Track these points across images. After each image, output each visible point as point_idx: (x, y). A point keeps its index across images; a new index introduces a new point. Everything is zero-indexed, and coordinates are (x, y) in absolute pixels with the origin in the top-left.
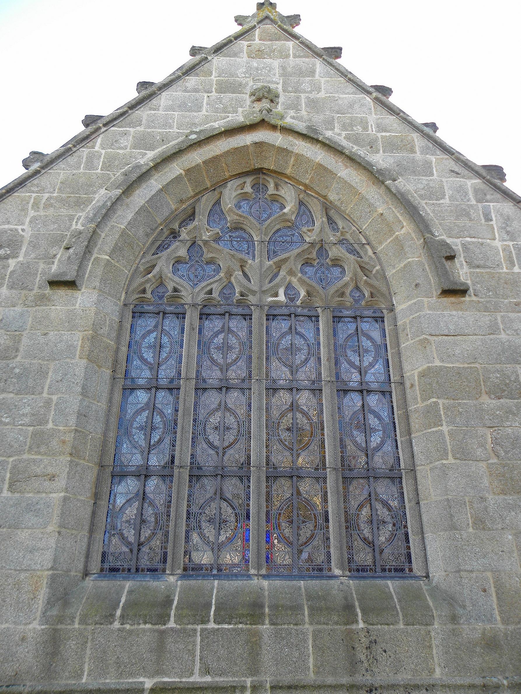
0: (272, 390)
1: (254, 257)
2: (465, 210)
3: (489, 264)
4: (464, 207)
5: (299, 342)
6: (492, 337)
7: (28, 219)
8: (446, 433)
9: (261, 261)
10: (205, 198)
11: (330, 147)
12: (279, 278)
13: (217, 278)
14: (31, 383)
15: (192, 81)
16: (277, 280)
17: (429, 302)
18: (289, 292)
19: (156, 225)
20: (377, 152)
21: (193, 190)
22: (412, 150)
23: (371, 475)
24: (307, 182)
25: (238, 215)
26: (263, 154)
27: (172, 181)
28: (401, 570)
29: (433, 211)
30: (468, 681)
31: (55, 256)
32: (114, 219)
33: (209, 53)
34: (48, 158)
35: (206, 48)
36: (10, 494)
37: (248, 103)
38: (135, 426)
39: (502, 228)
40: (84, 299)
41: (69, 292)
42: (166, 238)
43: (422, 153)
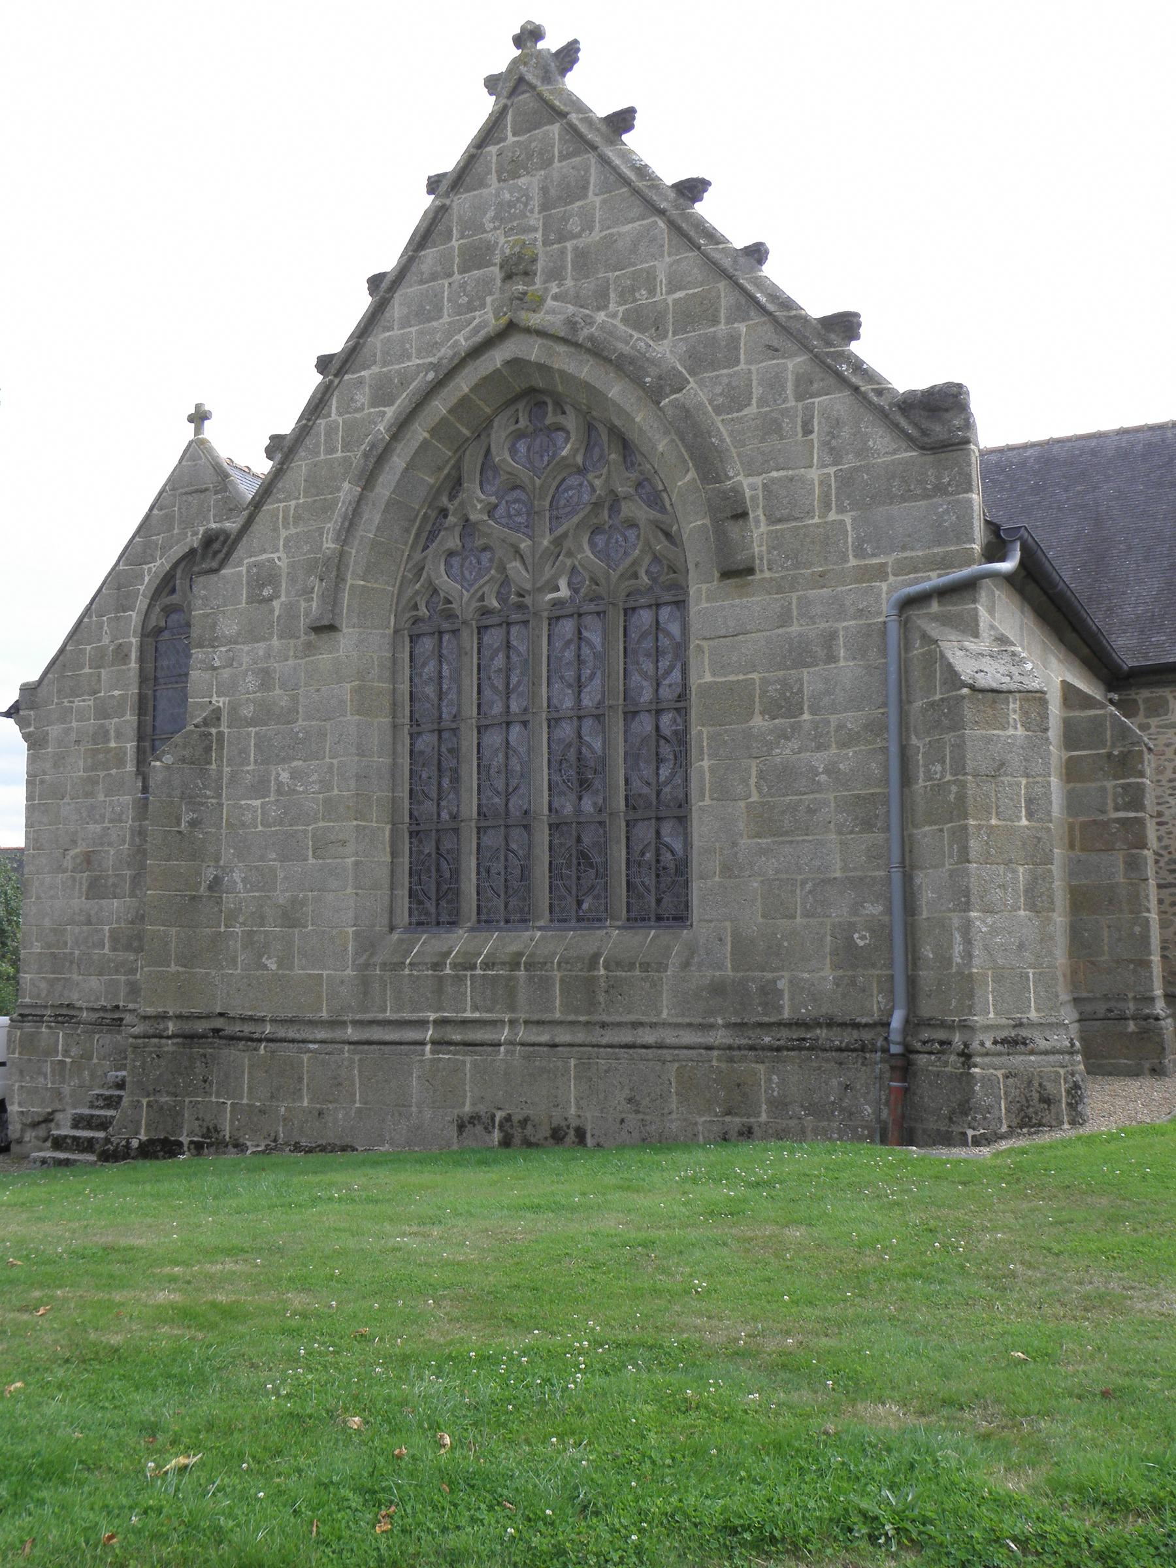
2: (775, 421)
4: (774, 415)
6: (780, 631)
8: (706, 769)
10: (468, 452)
11: (596, 351)
15: (430, 254)
17: (708, 589)
21: (449, 450)
27: (417, 453)
29: (731, 434)
30: (688, 1020)
32: (362, 527)
35: (445, 174)
36: (314, 861)
40: (347, 641)
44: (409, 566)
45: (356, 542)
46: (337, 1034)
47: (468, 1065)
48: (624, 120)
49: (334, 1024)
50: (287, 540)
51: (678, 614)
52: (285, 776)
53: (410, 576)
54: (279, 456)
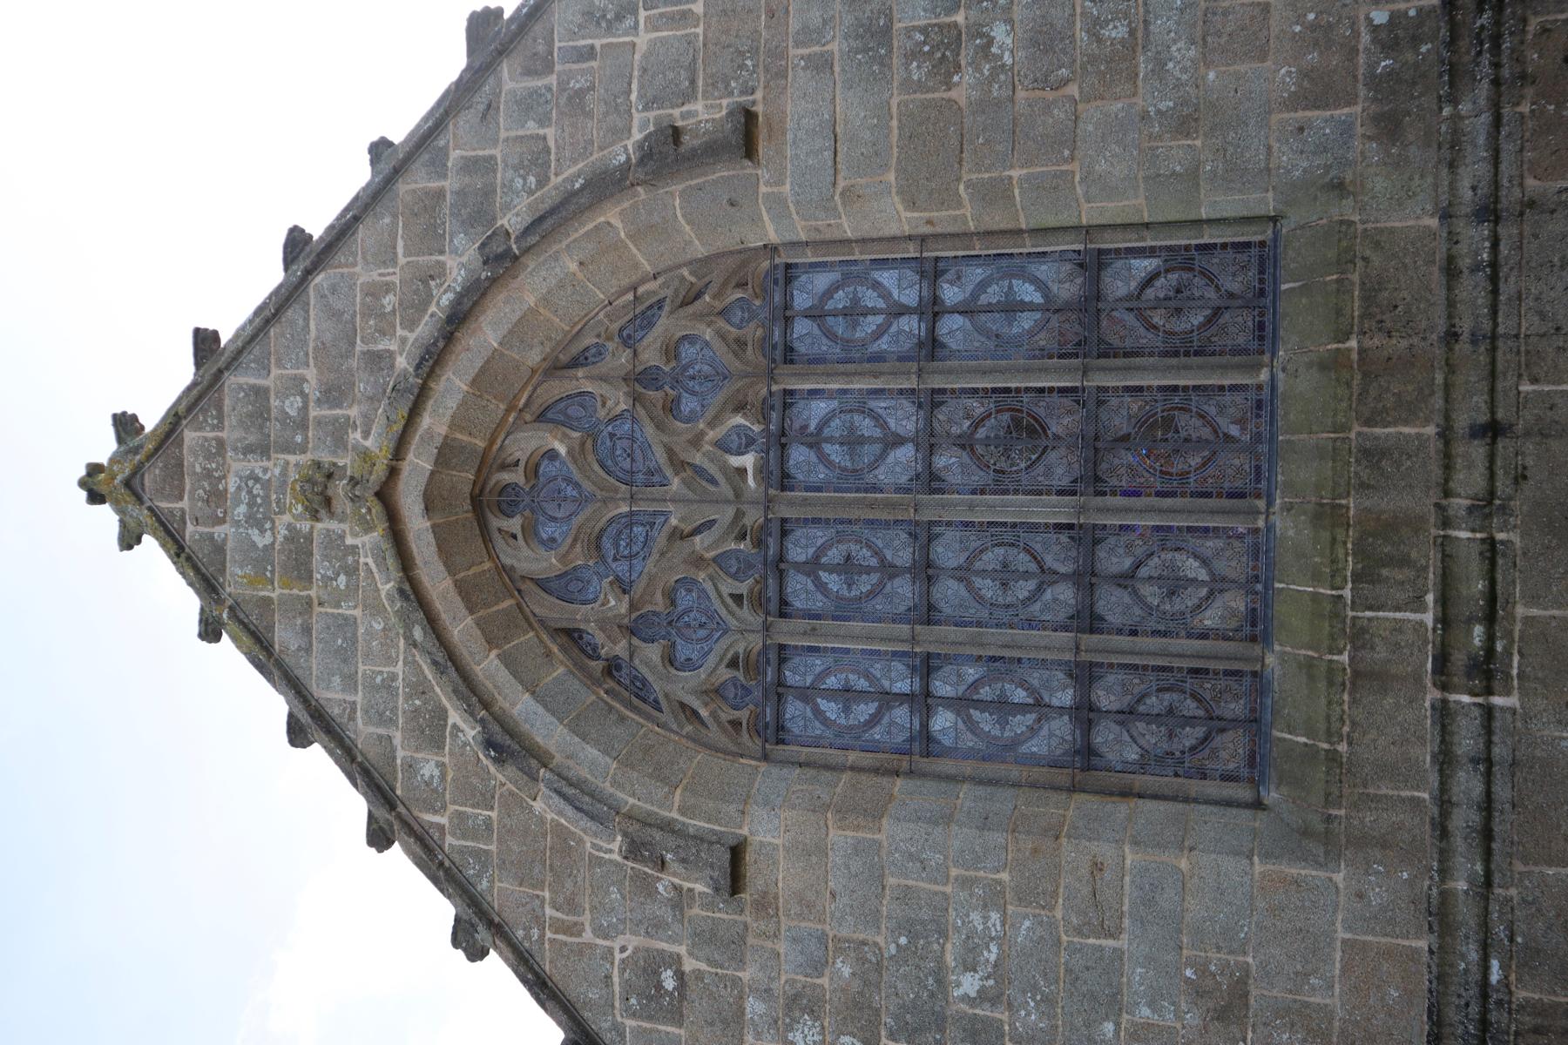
0: (931, 481)
1: (662, 513)
2: (570, 98)
3: (686, 60)
4: (563, 101)
5: (835, 428)
7: (599, 941)
9: (673, 501)
10: (537, 611)
11: (433, 360)
12: (707, 465)
13: (708, 586)
14: (925, 914)
15: (284, 637)
16: (713, 470)
17: (767, 183)
18: (734, 446)
19: (602, 704)
20: (442, 265)
21: (525, 632)
22: (440, 194)
23: (1091, 303)
24: (502, 407)
25: (573, 546)
26: (445, 494)
27: (515, 674)
28: (1264, 258)
29: (574, 161)
31: (675, 887)
32: (598, 782)
33: (219, 601)
34: (469, 914)
36: (1125, 936)
37: (333, 525)
38: (998, 733)
39: (609, 28)
40: (767, 831)
41: (749, 857)
42: (619, 683)
43: (445, 176)
44: (675, 727)
45: (620, 795)
46: (1466, 913)
47: (1535, 612)
48: (204, 340)
49: (1440, 917)
50: (601, 932)
51: (804, 278)
52: (969, 984)
53: (689, 728)
54: (483, 935)
